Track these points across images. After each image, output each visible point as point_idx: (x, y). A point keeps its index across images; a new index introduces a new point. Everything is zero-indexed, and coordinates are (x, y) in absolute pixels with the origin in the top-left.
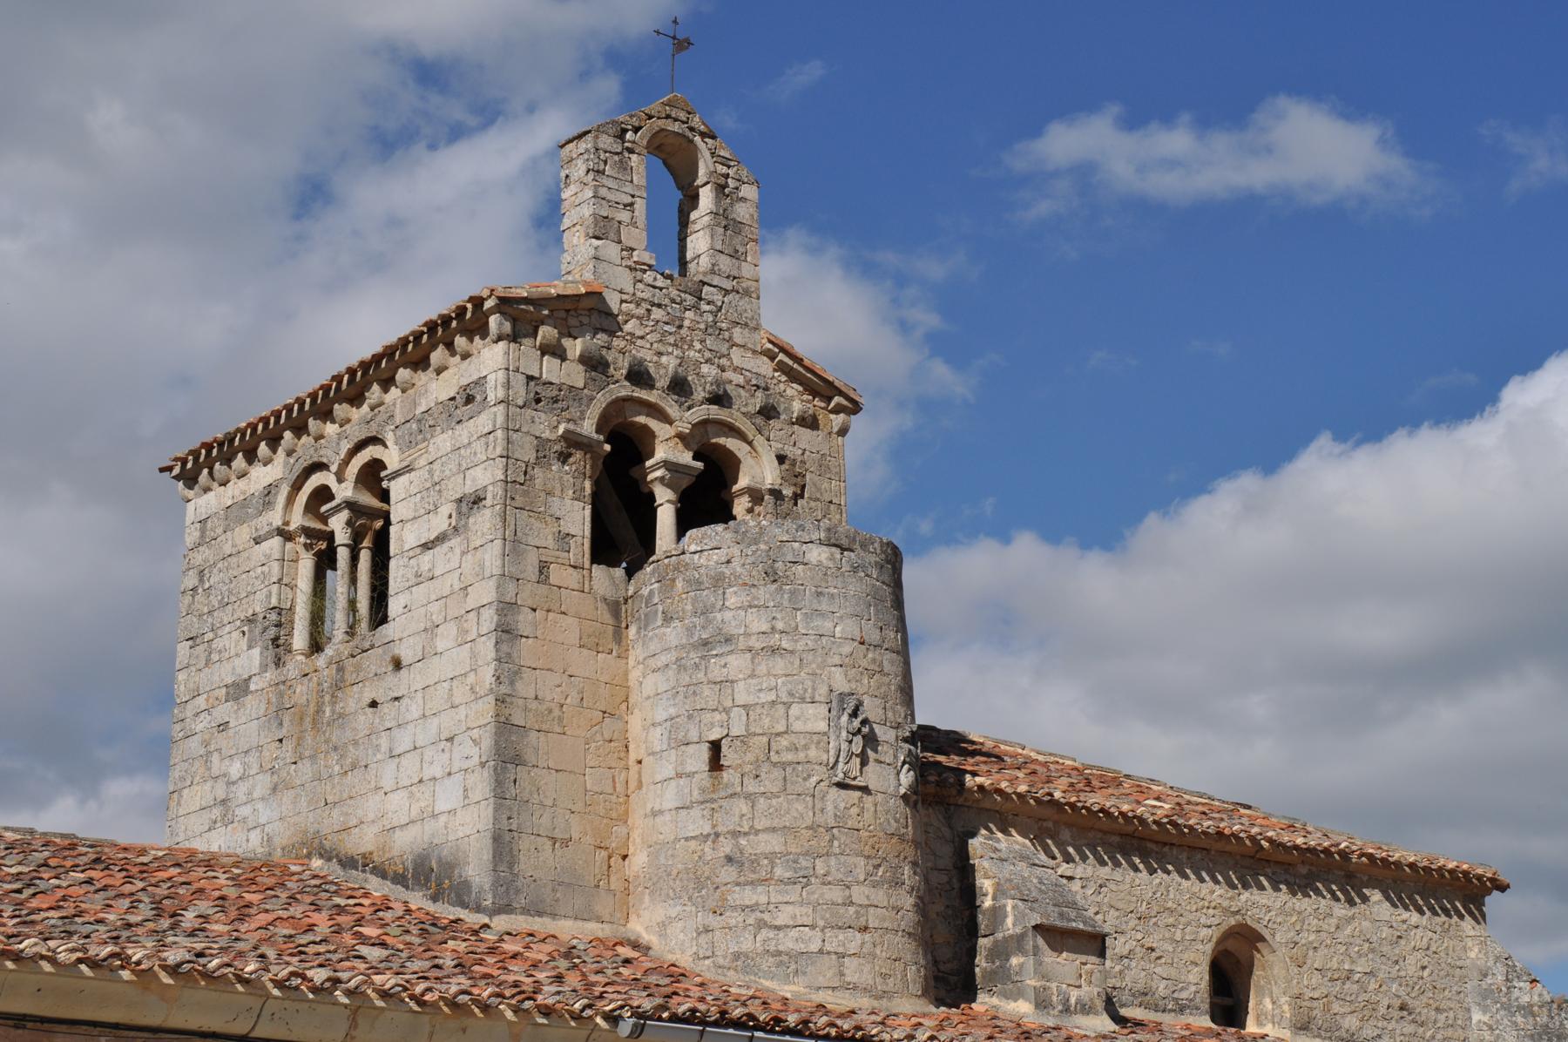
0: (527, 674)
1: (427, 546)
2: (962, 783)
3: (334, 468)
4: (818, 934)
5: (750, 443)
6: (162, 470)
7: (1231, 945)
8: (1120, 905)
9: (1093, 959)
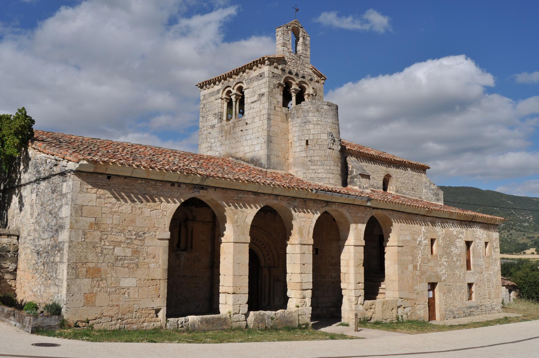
0: (272, 126)
1: (252, 103)
2: (346, 148)
3: (232, 87)
4: (325, 174)
5: (308, 85)
6: (196, 85)
7: (386, 177)
8: (369, 170)
9: (368, 180)
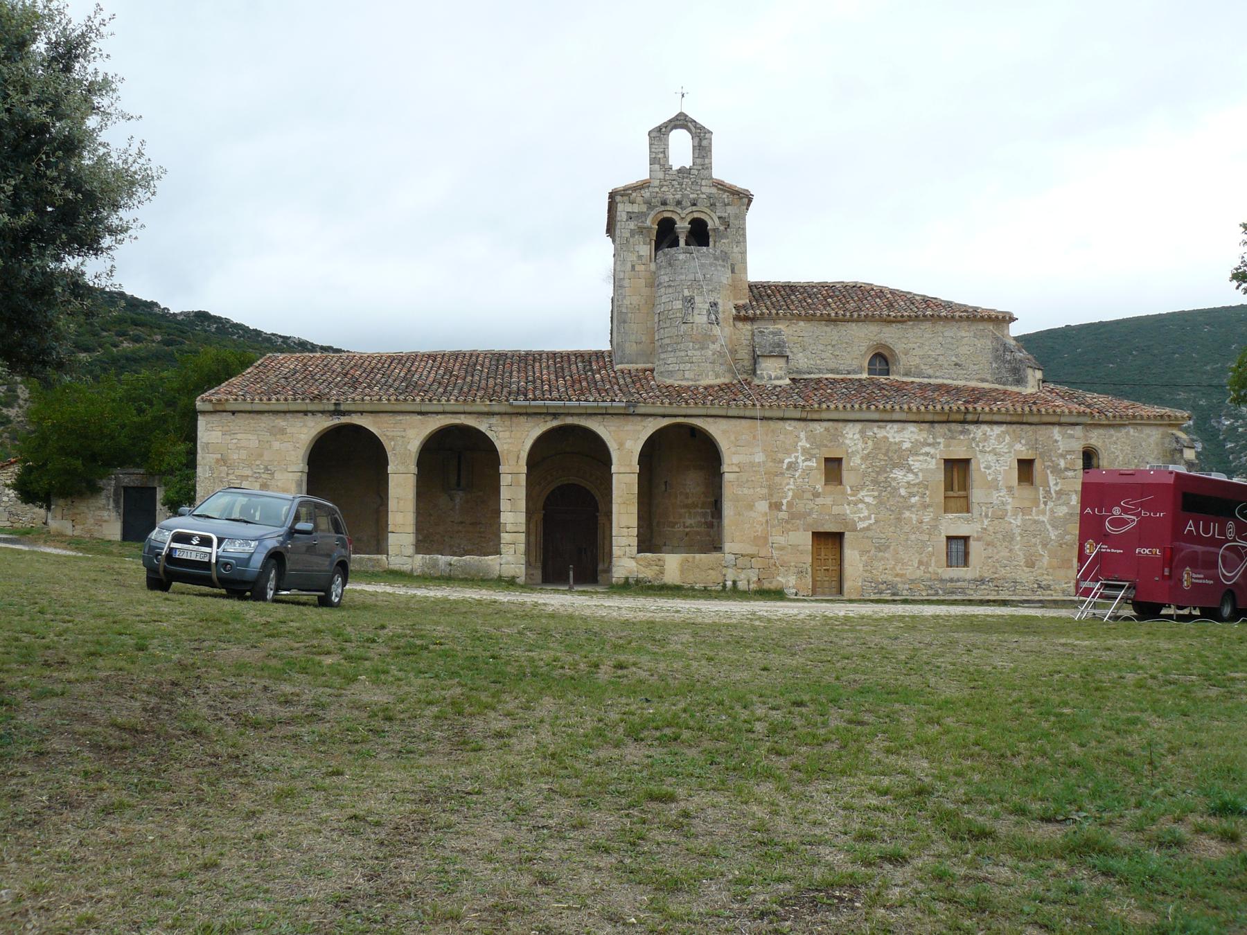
0: (628, 298)
